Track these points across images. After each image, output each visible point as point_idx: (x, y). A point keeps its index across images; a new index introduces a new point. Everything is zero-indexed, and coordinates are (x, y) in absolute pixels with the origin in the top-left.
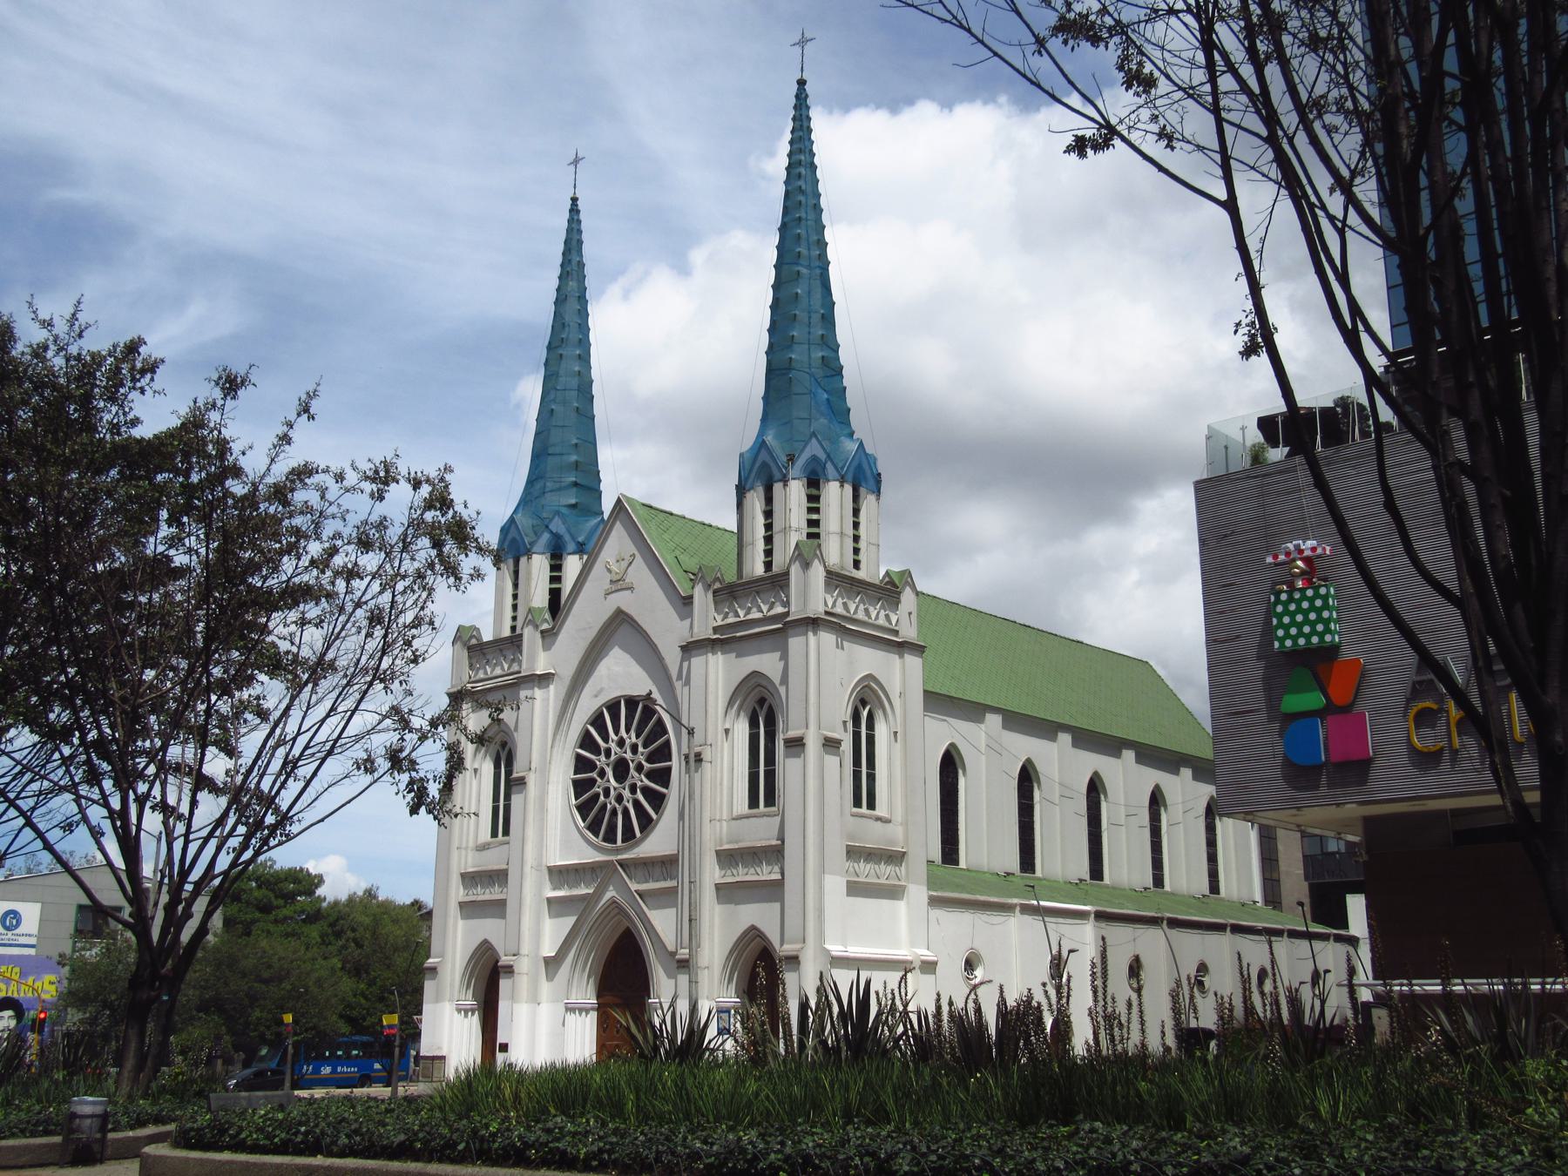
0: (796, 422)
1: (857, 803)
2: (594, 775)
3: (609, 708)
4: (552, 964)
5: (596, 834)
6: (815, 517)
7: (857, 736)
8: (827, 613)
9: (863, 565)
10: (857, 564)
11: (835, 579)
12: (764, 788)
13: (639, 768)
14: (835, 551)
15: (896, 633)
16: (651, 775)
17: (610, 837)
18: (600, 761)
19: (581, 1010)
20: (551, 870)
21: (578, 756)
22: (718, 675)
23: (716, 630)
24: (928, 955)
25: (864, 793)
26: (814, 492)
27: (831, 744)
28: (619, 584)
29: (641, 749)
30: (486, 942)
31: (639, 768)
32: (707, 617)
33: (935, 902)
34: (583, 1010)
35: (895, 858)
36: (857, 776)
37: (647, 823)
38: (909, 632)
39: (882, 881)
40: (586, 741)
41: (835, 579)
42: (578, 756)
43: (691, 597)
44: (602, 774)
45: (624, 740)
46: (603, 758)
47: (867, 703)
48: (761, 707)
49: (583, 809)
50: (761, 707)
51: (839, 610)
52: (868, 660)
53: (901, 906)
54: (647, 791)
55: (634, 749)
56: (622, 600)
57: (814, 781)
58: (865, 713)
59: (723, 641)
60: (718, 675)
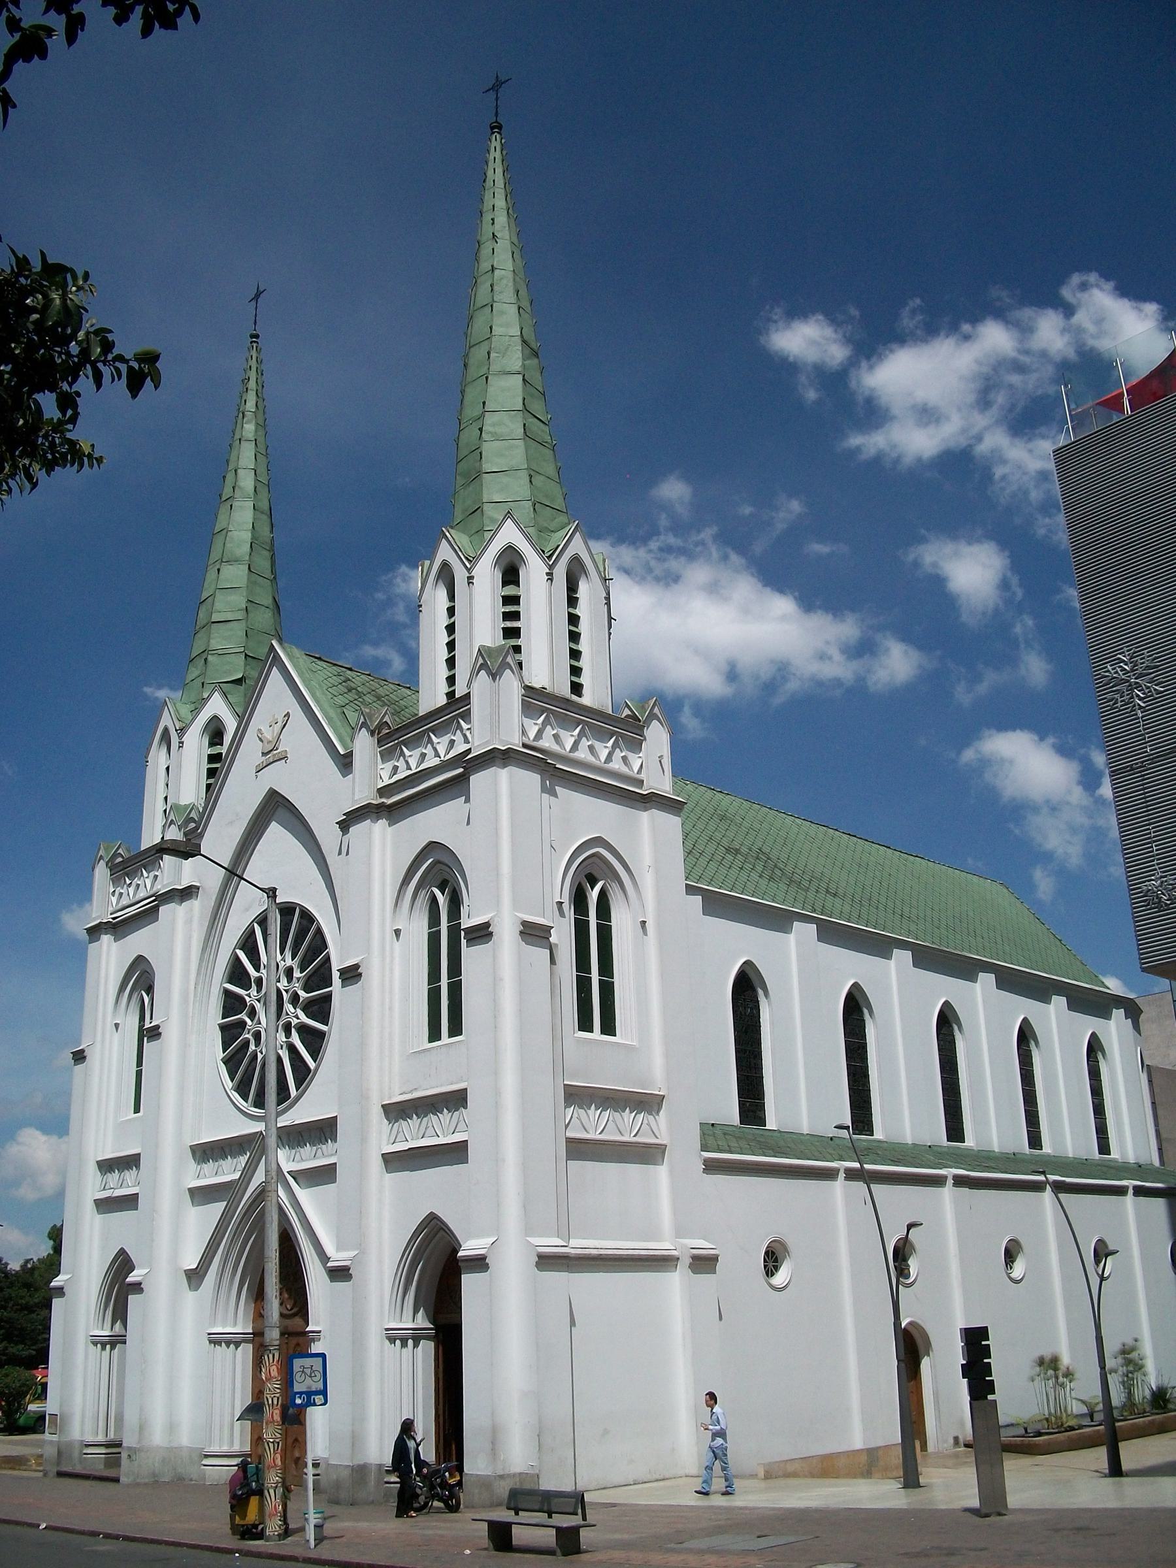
0: (486, 507)
1: (585, 1024)
2: (243, 1016)
3: (260, 924)
4: (194, 1277)
5: (245, 1097)
6: (509, 624)
7: (581, 929)
8: (525, 746)
9: (586, 691)
10: (577, 688)
11: (535, 700)
12: (446, 1012)
13: (295, 999)
14: (543, 665)
15: (640, 783)
16: (308, 1008)
17: (260, 1103)
18: (250, 996)
19: (228, 1343)
20: (192, 1191)
21: (227, 992)
22: (386, 849)
23: (382, 792)
24: (703, 1245)
25: (596, 1007)
26: (510, 591)
27: (534, 933)
28: (273, 755)
29: (297, 974)
30: (122, 1249)
31: (295, 999)
32: (374, 771)
33: (712, 1167)
34: (232, 1342)
35: (647, 1103)
36: (583, 985)
37: (303, 1074)
38: (661, 782)
39: (626, 1138)
40: (237, 974)
41: (535, 700)
42: (227, 992)
43: (350, 755)
44: (252, 1013)
45: (277, 961)
46: (253, 991)
47: (593, 882)
48: (438, 876)
49: (231, 1063)
50: (438, 876)
51: (547, 743)
52: (593, 817)
53: (661, 1173)
54: (303, 1029)
55: (289, 972)
56: (278, 778)
57: (511, 985)
58: (594, 895)
59: (392, 806)
60: (386, 849)
